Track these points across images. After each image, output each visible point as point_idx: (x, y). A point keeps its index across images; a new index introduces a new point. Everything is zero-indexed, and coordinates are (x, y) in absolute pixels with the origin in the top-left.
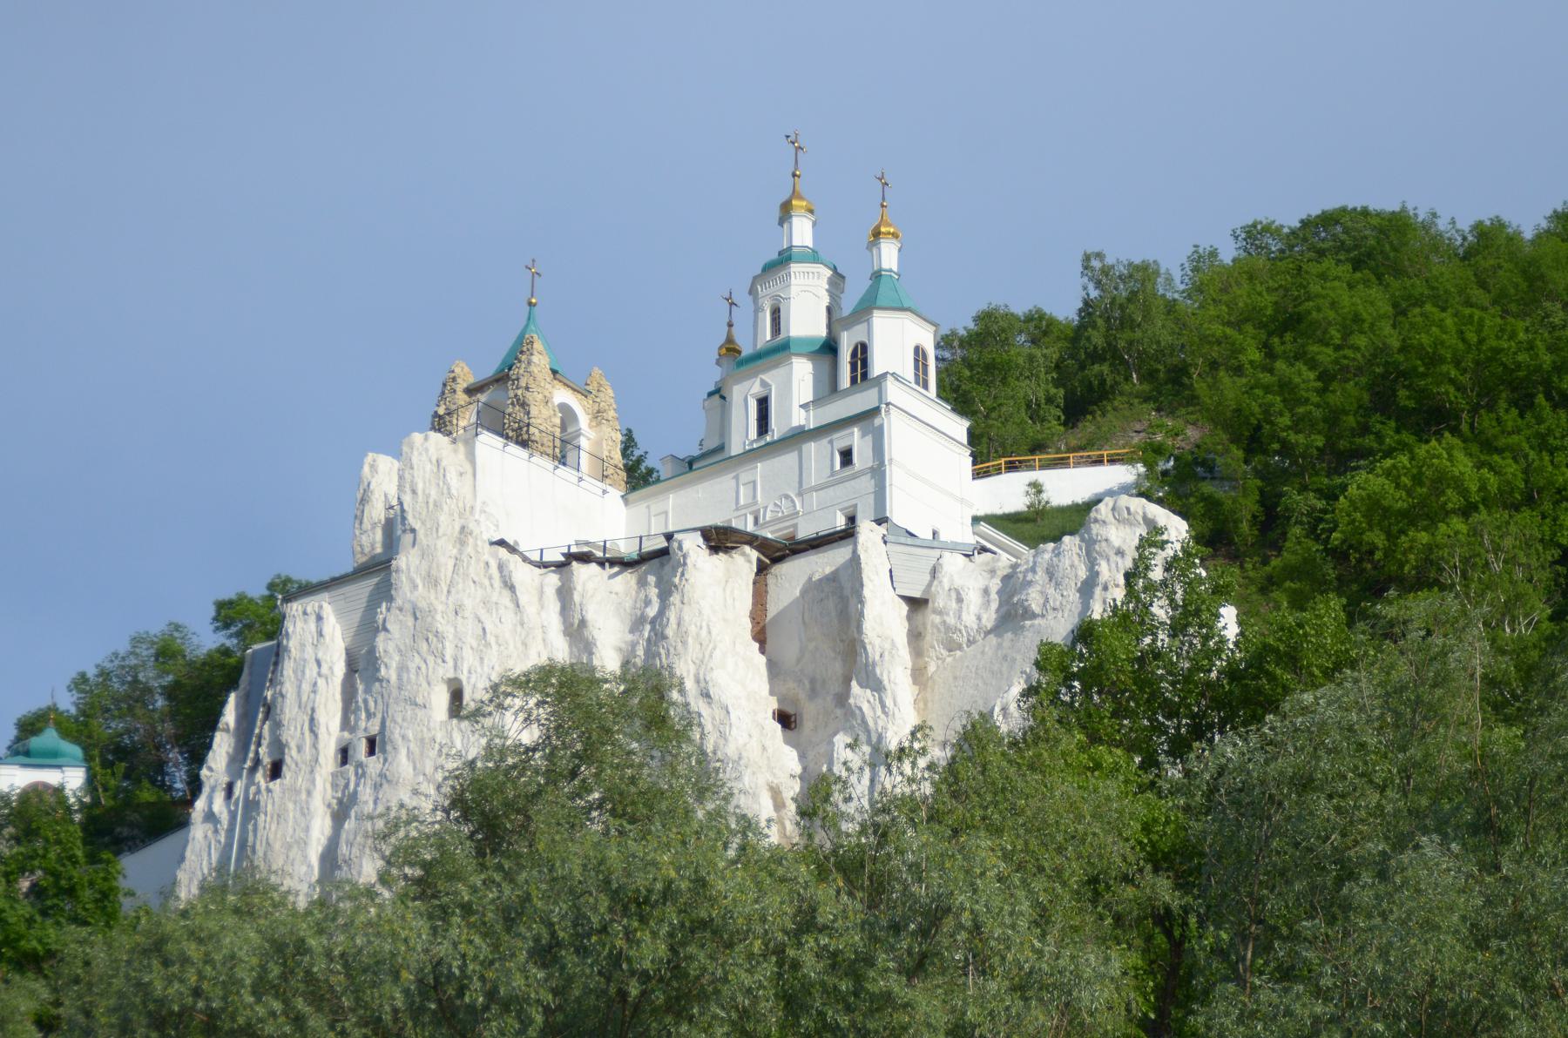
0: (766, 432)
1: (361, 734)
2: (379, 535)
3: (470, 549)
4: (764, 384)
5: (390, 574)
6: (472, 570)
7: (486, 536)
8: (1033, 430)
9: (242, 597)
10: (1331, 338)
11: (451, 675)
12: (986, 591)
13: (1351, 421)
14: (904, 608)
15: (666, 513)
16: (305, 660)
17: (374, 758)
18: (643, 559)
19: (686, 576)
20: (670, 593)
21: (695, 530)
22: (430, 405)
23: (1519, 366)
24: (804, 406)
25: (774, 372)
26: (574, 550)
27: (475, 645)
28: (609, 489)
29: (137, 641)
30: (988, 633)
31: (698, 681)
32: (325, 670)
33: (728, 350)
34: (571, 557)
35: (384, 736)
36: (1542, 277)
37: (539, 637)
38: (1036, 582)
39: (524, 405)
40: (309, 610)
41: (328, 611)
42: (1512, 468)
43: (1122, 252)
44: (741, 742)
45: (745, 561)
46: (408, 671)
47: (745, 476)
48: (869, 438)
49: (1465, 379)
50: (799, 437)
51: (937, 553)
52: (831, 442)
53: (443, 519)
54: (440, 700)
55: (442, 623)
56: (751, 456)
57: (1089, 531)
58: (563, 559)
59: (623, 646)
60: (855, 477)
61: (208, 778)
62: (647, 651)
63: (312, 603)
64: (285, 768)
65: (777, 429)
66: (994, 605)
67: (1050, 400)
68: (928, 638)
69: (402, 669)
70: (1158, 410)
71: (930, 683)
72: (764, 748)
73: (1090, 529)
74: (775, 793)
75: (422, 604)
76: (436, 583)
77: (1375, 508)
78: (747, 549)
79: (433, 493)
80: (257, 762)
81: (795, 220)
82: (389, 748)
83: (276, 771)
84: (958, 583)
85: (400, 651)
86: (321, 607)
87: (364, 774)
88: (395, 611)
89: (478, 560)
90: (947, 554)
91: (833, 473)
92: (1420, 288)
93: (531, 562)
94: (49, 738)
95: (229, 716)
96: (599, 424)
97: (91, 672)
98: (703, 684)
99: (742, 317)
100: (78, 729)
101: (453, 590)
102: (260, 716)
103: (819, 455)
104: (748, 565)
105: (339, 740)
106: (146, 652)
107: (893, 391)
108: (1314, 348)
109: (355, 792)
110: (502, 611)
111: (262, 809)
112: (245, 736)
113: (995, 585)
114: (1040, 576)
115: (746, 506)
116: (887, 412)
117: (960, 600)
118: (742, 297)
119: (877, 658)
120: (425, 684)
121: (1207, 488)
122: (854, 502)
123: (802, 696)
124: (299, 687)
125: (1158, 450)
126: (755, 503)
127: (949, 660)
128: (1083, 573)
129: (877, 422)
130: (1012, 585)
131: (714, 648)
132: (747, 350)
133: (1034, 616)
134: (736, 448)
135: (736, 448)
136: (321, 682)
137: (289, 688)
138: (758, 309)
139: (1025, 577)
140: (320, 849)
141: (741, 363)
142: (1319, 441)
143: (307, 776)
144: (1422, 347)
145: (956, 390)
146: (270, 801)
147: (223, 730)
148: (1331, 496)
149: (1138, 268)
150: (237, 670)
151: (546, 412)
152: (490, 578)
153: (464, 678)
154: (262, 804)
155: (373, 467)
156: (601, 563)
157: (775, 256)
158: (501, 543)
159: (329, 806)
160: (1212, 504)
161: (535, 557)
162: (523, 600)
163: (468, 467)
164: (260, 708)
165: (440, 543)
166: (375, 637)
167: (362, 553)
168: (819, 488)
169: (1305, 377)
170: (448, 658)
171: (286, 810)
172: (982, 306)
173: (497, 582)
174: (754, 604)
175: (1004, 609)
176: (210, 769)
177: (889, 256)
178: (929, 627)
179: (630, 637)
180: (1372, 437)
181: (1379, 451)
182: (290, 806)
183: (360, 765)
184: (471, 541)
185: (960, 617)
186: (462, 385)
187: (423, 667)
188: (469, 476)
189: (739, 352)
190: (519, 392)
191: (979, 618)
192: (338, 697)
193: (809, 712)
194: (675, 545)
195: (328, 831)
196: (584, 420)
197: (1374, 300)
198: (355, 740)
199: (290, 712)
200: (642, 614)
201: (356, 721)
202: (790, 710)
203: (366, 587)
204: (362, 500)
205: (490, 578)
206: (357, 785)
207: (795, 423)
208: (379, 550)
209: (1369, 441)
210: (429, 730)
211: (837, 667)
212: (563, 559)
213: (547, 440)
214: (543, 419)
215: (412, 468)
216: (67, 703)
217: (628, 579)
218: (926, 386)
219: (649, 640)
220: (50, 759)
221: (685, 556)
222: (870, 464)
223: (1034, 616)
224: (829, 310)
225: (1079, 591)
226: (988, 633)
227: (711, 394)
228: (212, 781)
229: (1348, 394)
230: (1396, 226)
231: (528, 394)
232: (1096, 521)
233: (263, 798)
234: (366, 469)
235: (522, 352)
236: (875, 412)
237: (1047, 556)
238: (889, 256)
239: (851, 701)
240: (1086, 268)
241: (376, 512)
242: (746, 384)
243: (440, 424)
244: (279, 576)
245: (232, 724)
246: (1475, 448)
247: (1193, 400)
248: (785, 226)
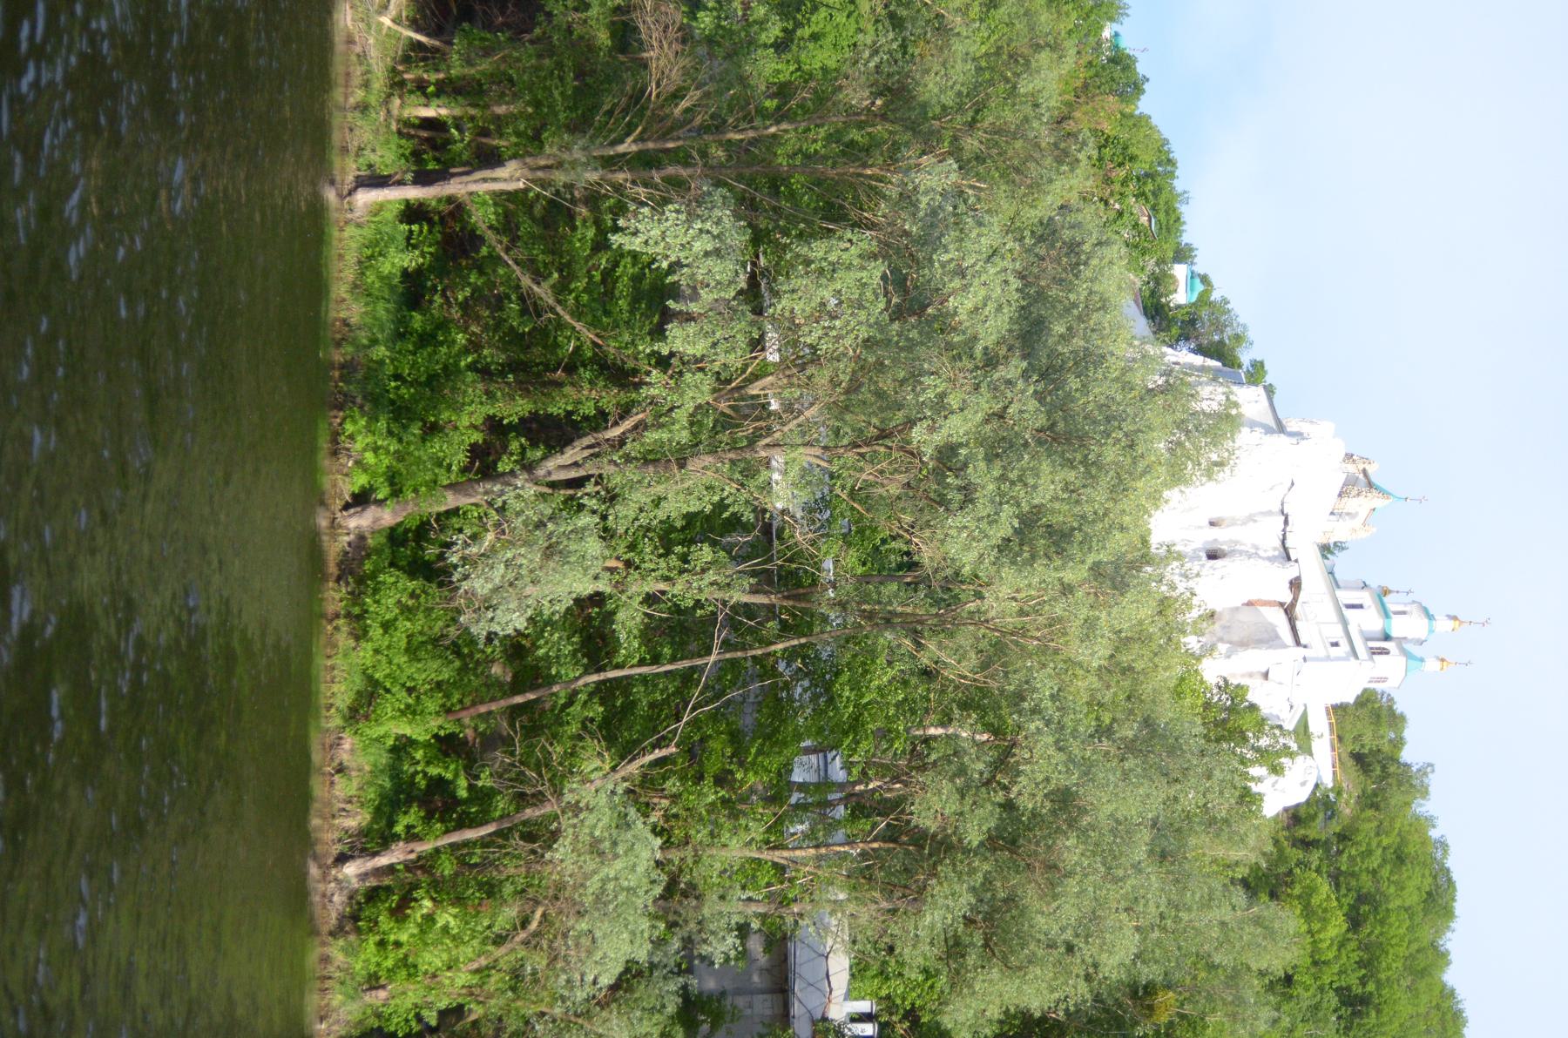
8: (1349, 737)
9: (1266, 372)
14: (1264, 670)
18: (1286, 549)
22: (1357, 453)
23: (1379, 963)
29: (1244, 326)
36: (1423, 977)
42: (1331, 955)
43: (1434, 782)
45: (1287, 598)
49: (1373, 938)
50: (1344, 623)
56: (1336, 600)
65: (1348, 613)
67: (1363, 746)
77: (1311, 891)
92: (1417, 920)
94: (1200, 287)
97: (1229, 306)
99: (1402, 597)
100: (1203, 299)
103: (1337, 633)
106: (1239, 331)
108: (1388, 867)
118: (1411, 597)
121: (1321, 816)
125: (1339, 793)
129: (1352, 659)
132: (1386, 599)
135: (1339, 593)
138: (1405, 604)
141: (1379, 596)
142: (1343, 868)
145: (1368, 700)
148: (1318, 871)
149: (1427, 789)
150: (1232, 366)
156: (1284, 530)
160: (1313, 817)
169: (1374, 862)
172: (1408, 716)
177: (1432, 665)
197: (1412, 898)
203: (1273, 424)
209: (1343, 891)
211: (1235, 638)
213: (1342, 506)
214: (1351, 504)
216: (1215, 296)
217: (1278, 543)
220: (1190, 288)
229: (1366, 882)
230: (1448, 913)
236: (1356, 656)
243: (1349, 457)
246: (1340, 939)
247: (1362, 810)
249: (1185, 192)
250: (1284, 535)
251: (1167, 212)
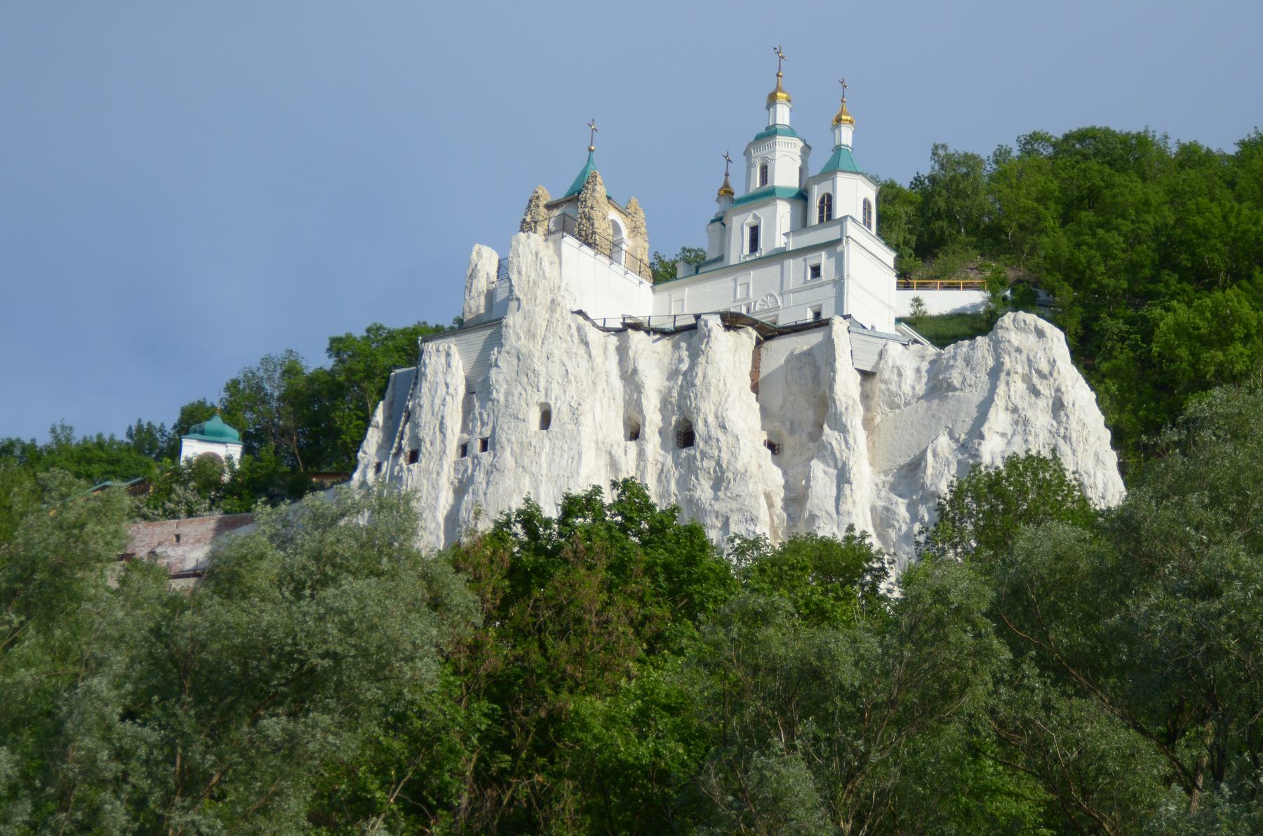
0: (756, 250)
1: (477, 436)
2: (482, 301)
3: (557, 315)
4: (756, 217)
5: (501, 328)
6: (559, 329)
7: (569, 307)
9: (349, 336)
10: (1130, 215)
11: (543, 400)
12: (918, 370)
13: (1147, 272)
14: (858, 377)
15: (683, 301)
16: (437, 383)
17: (486, 453)
18: (678, 331)
19: (710, 344)
20: (698, 356)
21: (715, 313)
24: (786, 235)
25: (764, 210)
26: (628, 321)
27: (560, 381)
28: (644, 281)
30: (920, 398)
31: (717, 417)
32: (451, 390)
33: (725, 192)
34: (627, 326)
35: (494, 439)
37: (604, 378)
38: (957, 367)
39: (589, 219)
40: (441, 348)
41: (454, 350)
43: (958, 146)
44: (746, 460)
45: (748, 337)
46: (513, 395)
47: (741, 278)
48: (833, 260)
50: (780, 255)
51: (884, 341)
52: (805, 260)
53: (539, 293)
54: (535, 417)
55: (538, 364)
57: (996, 334)
58: (621, 326)
59: (662, 389)
60: (821, 285)
61: (363, 458)
62: (680, 394)
63: (443, 344)
64: (421, 456)
65: (764, 249)
66: (924, 380)
68: (876, 399)
69: (508, 394)
70: (982, 255)
71: (877, 430)
72: (760, 466)
73: (997, 333)
74: (768, 497)
75: (524, 350)
76: (534, 337)
78: (750, 329)
79: (533, 274)
80: (400, 449)
81: (779, 106)
82: (498, 447)
83: (414, 457)
84: (899, 363)
85: (507, 381)
86: (449, 347)
87: (479, 463)
88: (504, 354)
89: (563, 324)
90: (890, 343)
91: (806, 281)
93: (598, 327)
95: (379, 416)
96: (636, 235)
98: (720, 420)
100: (230, 414)
101: (546, 343)
102: (403, 419)
103: (796, 269)
104: (749, 340)
105: (460, 439)
107: (851, 229)
109: (472, 475)
110: (579, 359)
111: (404, 482)
112: (391, 432)
113: (925, 366)
114: (960, 363)
115: (741, 300)
116: (847, 242)
117: (900, 375)
118: (739, 161)
119: (843, 410)
120: (524, 405)
122: (820, 303)
123: (784, 432)
124: (433, 401)
126: (749, 298)
127: (891, 415)
128: (991, 363)
129: (839, 249)
130: (936, 369)
131: (729, 395)
132: (739, 193)
133: (955, 389)
134: (734, 259)
135: (734, 259)
136: (448, 399)
137: (425, 401)
138: (750, 166)
139: (948, 362)
140: (445, 513)
143: (437, 462)
144: (1195, 225)
146: (410, 478)
147: (375, 426)
151: (604, 225)
152: (572, 336)
153: (552, 403)
154: (404, 478)
155: (479, 254)
157: (762, 130)
158: (580, 312)
159: (452, 483)
161: (600, 324)
162: (594, 352)
163: (556, 259)
164: (401, 414)
165: (537, 309)
166: (489, 370)
167: (470, 312)
168: (795, 291)
170: (541, 388)
171: (422, 485)
173: (576, 339)
174: (753, 367)
175: (932, 383)
176: (365, 453)
177: (846, 136)
178: (877, 391)
179: (667, 384)
180: (1162, 285)
181: (1166, 294)
182: (425, 482)
183: (476, 457)
184: (559, 309)
185: (900, 387)
186: (543, 202)
187: (524, 393)
188: (557, 265)
189: (733, 194)
190: (586, 210)
191: (913, 388)
192: (460, 410)
193: (789, 443)
194: (702, 323)
195: (451, 501)
196: (625, 233)
198: (473, 440)
199: (426, 417)
200: (677, 368)
201: (473, 428)
202: (775, 441)
203: (479, 338)
204: (471, 276)
205: (572, 336)
206: (474, 471)
207: (777, 246)
208: (482, 311)
209: (1161, 287)
210: (527, 437)
211: (810, 415)
212: (621, 326)
214: (601, 226)
215: (518, 256)
217: (664, 345)
218: (869, 227)
219: (681, 387)
221: (709, 331)
222: (833, 278)
223: (955, 389)
224: (801, 170)
225: (988, 374)
226: (920, 398)
227: (713, 221)
228: (365, 461)
229: (1146, 253)
231: (592, 212)
232: (1001, 327)
233: (405, 475)
234: (474, 255)
235: (588, 183)
236: (839, 241)
237: (965, 349)
238: (846, 136)
239: (824, 438)
240: (934, 154)
241: (481, 284)
242: (742, 216)
244: (375, 324)
245: (381, 423)
248: (771, 110)
249: (53, 431)
250: (656, 331)
251: (89, 462)
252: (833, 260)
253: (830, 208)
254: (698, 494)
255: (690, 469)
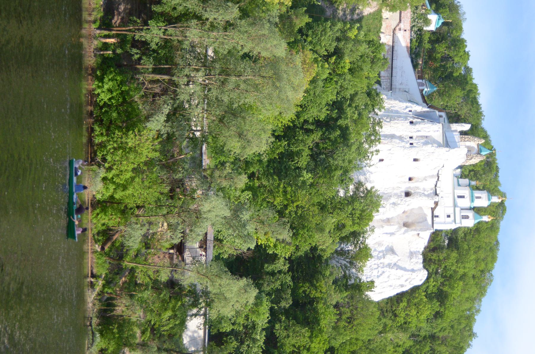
60: (445, 218)
83: (411, 123)
103: (450, 211)
114: (417, 261)
129: (454, 223)
133: (410, 260)
137: (427, 125)
164: (422, 116)
223: (410, 260)
252: (451, 221)
253: (465, 218)
254: (392, 198)
255: (399, 196)
